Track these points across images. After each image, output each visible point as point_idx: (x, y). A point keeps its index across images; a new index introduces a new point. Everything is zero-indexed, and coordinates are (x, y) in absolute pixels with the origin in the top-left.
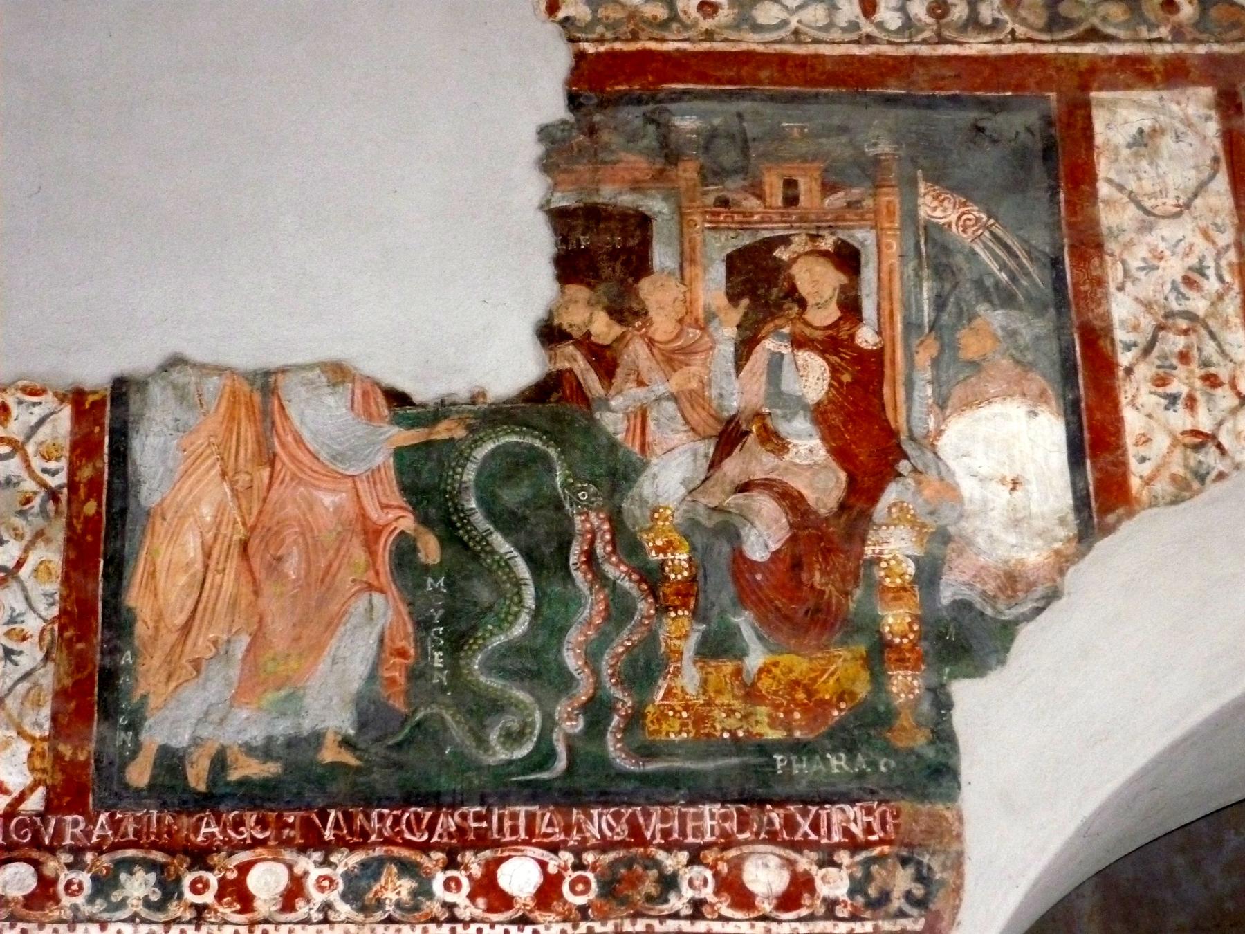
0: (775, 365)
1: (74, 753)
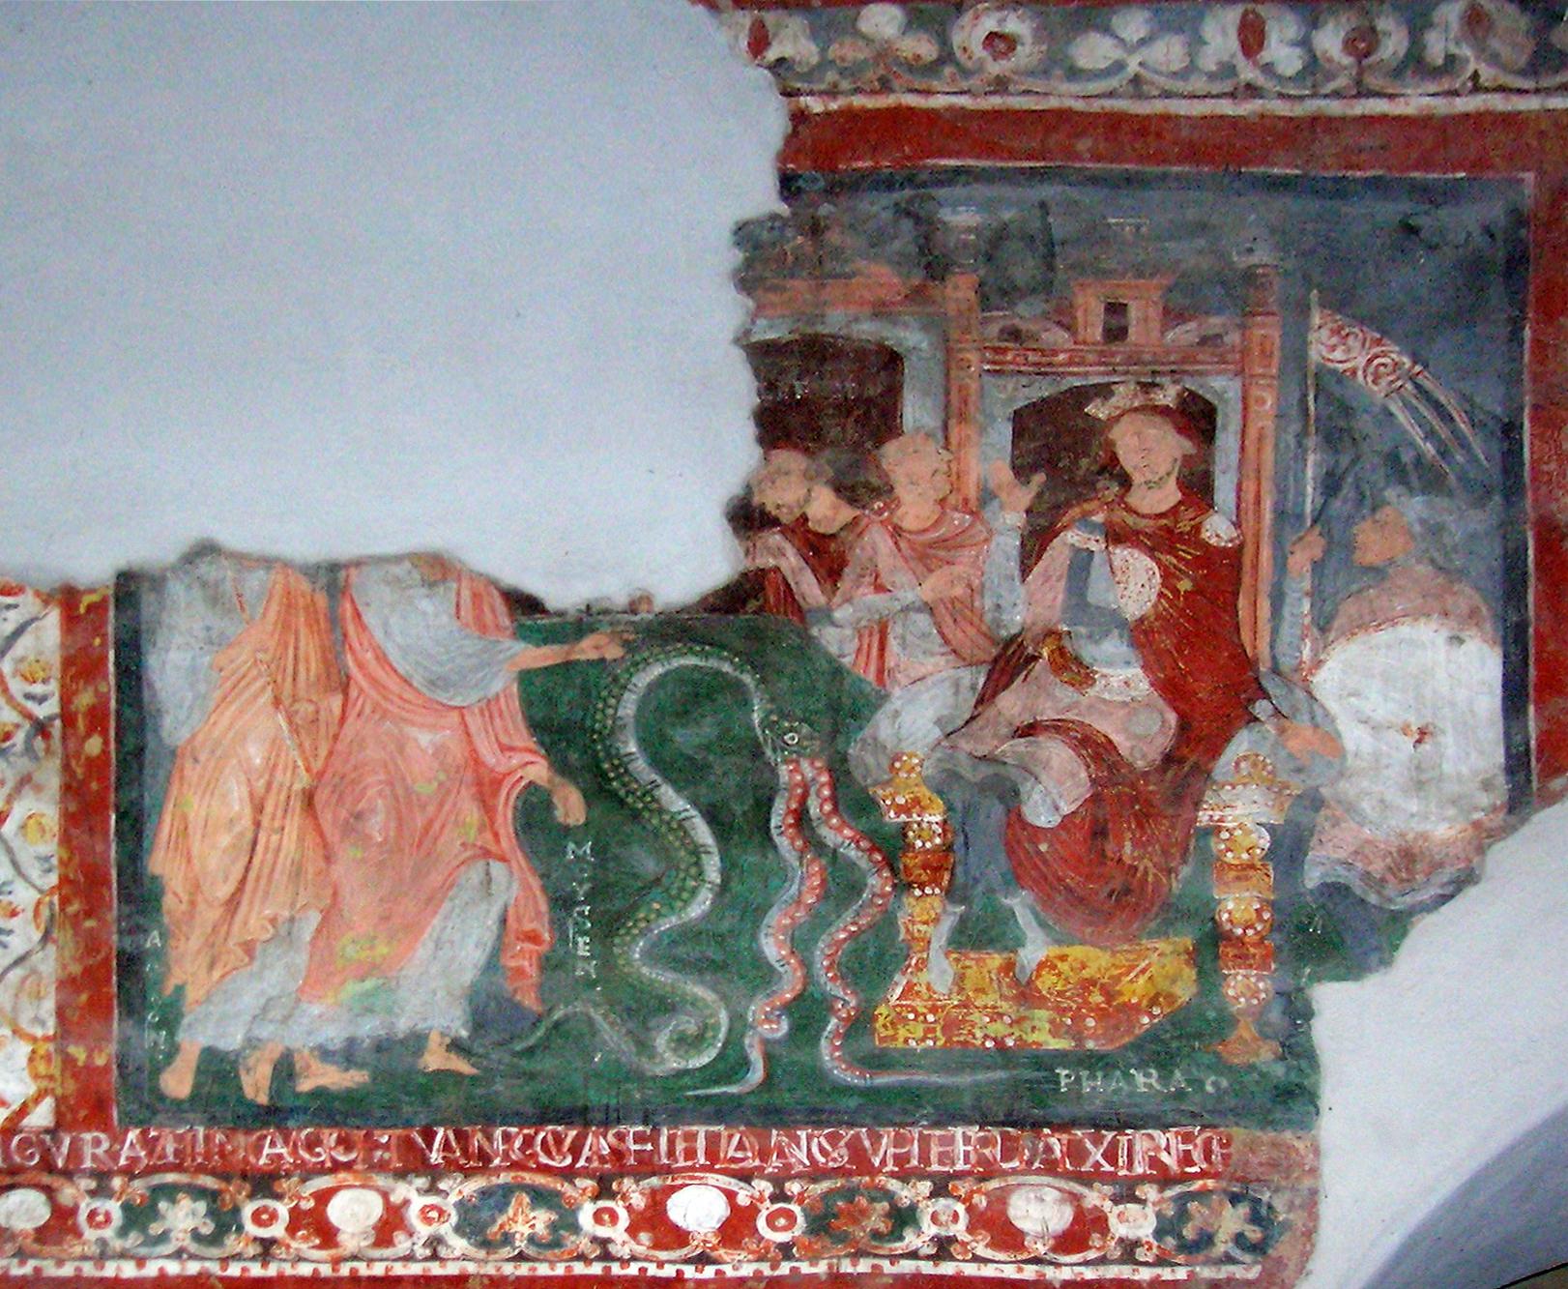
0: (1081, 565)
1: (90, 1056)
